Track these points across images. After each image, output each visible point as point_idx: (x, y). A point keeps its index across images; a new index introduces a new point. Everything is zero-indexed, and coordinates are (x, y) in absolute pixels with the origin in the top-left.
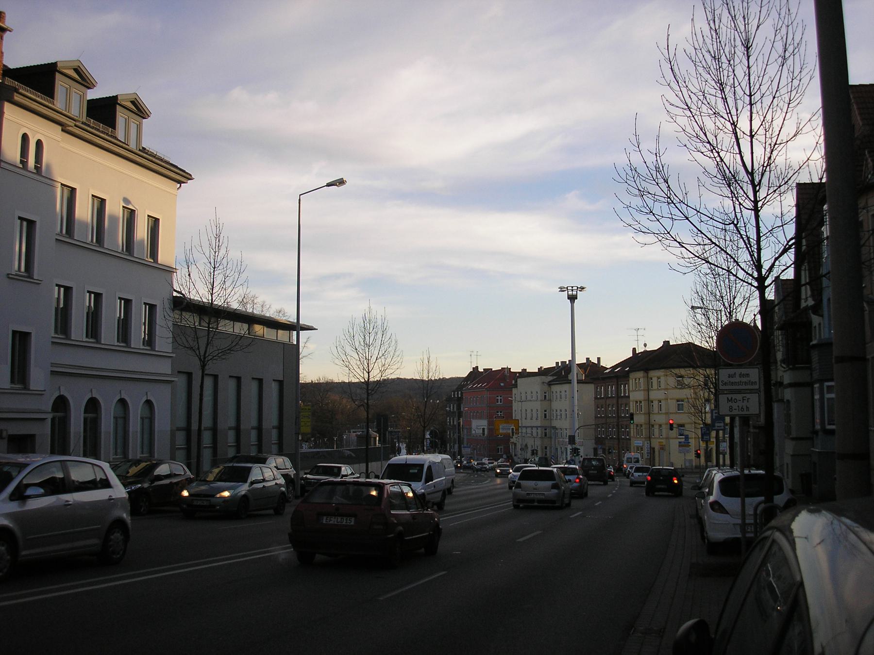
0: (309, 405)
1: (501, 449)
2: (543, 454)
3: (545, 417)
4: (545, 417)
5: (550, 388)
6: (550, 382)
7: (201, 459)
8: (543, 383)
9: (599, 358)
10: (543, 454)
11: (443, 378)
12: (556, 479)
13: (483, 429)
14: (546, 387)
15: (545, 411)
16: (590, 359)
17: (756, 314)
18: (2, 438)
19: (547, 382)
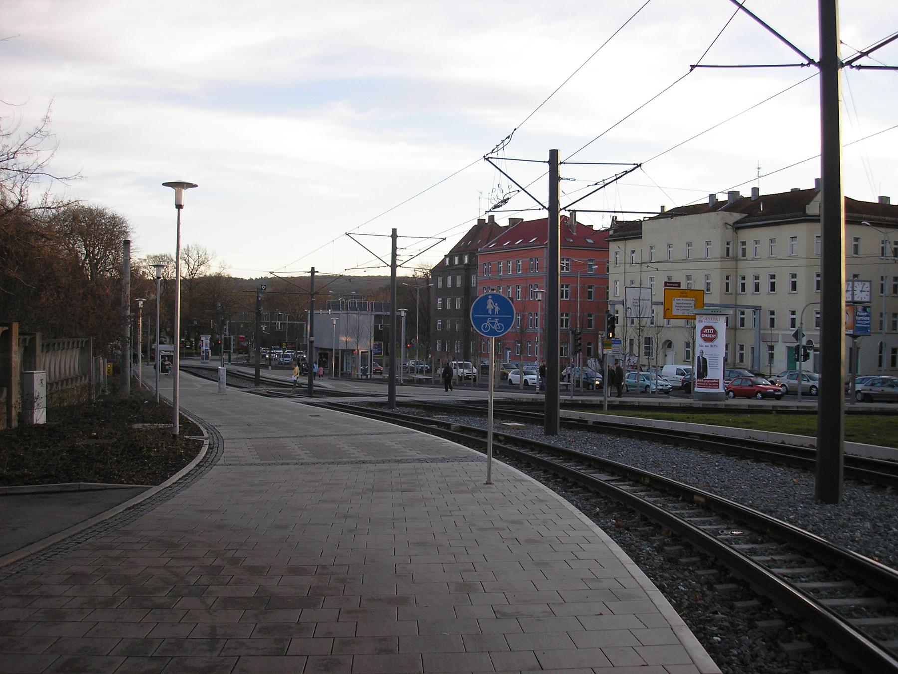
0: (288, 356)
1: (518, 354)
2: (694, 322)
3: (727, 290)
4: (727, 290)
5: (737, 233)
6: (737, 222)
7: (524, 401)
8: (726, 224)
9: (396, 229)
10: (694, 322)
11: (265, 277)
12: (769, 318)
13: (315, 379)
14: (730, 231)
15: (728, 278)
16: (258, 278)
17: (55, 201)
18: (1, 238)
19: (731, 223)
